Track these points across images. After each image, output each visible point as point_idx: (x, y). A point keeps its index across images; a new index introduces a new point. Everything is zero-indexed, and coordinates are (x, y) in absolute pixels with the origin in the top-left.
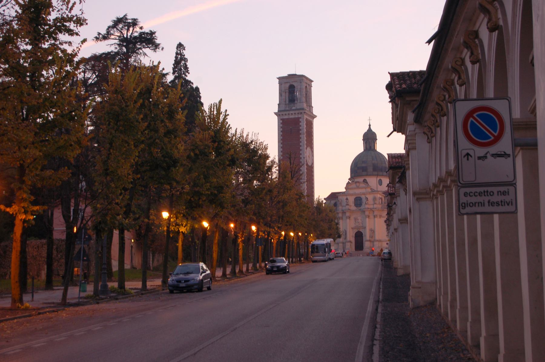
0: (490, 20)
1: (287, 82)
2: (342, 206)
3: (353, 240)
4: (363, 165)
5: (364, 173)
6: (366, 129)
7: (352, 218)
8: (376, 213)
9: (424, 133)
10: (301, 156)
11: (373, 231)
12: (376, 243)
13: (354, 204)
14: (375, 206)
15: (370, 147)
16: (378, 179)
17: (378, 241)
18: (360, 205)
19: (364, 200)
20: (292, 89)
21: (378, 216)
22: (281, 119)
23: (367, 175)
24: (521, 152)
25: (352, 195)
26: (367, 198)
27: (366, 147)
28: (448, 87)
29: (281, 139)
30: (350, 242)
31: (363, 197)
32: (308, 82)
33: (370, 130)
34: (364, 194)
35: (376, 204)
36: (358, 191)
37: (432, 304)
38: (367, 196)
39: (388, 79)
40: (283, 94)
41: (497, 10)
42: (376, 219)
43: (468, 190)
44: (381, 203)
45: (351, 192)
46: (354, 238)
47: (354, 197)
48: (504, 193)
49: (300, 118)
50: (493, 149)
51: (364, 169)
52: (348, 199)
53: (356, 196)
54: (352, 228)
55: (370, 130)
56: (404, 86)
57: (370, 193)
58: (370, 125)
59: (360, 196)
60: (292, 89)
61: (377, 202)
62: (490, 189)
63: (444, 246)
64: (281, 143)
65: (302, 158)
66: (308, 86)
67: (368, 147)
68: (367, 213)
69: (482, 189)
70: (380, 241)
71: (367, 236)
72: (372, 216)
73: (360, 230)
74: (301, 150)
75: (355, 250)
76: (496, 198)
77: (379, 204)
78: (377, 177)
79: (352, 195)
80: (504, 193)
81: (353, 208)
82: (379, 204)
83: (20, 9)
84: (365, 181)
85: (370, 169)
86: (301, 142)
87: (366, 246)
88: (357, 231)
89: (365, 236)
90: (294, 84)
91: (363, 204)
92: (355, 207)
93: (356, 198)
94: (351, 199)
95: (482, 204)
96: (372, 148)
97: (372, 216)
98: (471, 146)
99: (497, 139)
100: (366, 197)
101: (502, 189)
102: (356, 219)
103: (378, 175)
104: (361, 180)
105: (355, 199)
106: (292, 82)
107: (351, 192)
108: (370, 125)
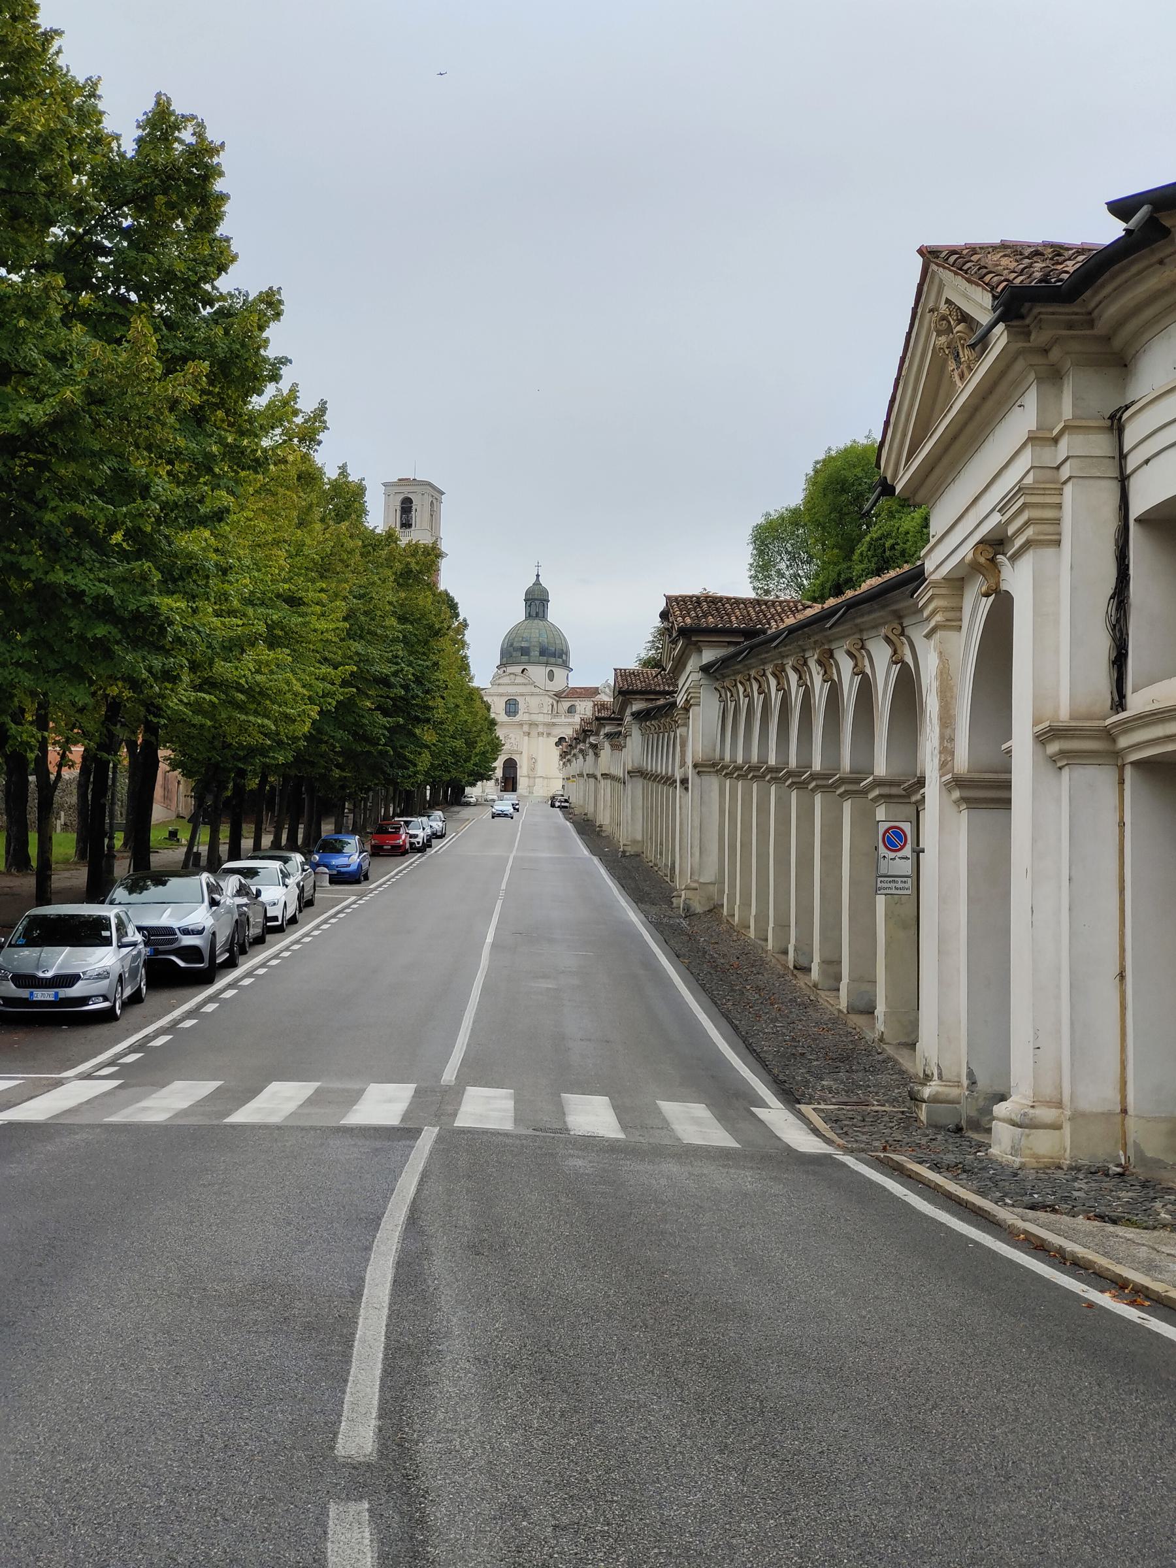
0: (856, 665)
4: (524, 644)
5: (525, 658)
9: (716, 689)
11: (533, 761)
15: (537, 614)
16: (548, 669)
18: (515, 713)
23: (529, 662)
25: (501, 695)
28: (777, 673)
32: (436, 495)
33: (537, 583)
34: (522, 695)
36: (512, 690)
37: (714, 910)
39: (662, 605)
41: (863, 657)
42: (541, 738)
43: (882, 879)
45: (501, 690)
48: (905, 882)
50: (900, 854)
51: (525, 651)
55: (537, 583)
56: (688, 620)
58: (538, 576)
62: (896, 879)
63: (746, 845)
66: (434, 501)
69: (891, 879)
76: (900, 885)
79: (501, 695)
80: (905, 882)
85: (535, 653)
95: (891, 889)
96: (541, 615)
98: (887, 851)
99: (903, 847)
101: (903, 879)
103: (547, 664)
107: (501, 690)
108: (538, 576)
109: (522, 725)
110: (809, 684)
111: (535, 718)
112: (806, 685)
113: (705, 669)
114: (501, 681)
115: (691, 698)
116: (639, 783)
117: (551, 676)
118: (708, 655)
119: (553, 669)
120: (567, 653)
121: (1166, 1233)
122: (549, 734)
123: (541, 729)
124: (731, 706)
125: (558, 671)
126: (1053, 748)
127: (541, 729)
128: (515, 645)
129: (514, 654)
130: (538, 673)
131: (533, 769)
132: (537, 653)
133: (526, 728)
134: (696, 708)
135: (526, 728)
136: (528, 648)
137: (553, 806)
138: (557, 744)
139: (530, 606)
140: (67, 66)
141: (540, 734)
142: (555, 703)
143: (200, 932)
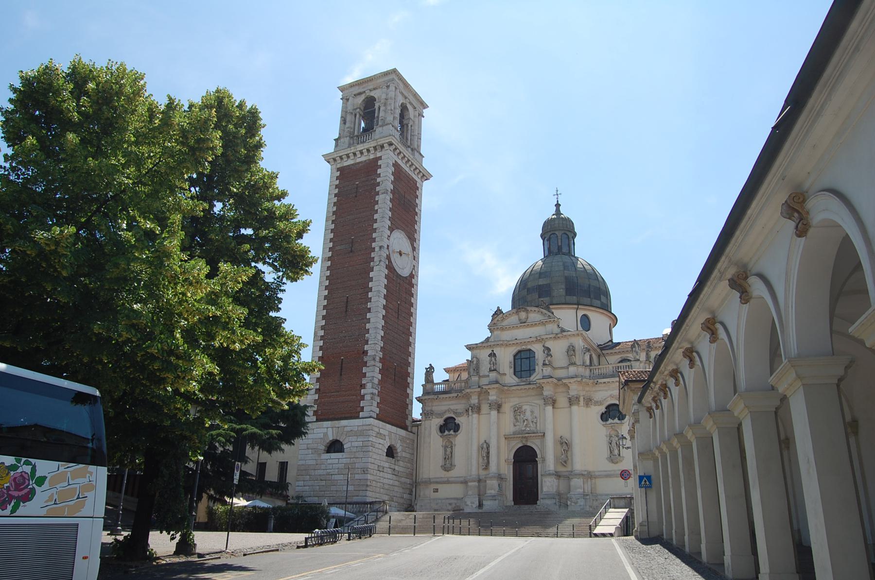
1: (360, 94)
2: (480, 377)
3: (508, 471)
6: (550, 213)
7: (507, 408)
8: (575, 389)
10: (374, 245)
11: (565, 445)
12: (576, 482)
13: (512, 370)
14: (572, 370)
15: (560, 249)
16: (581, 313)
17: (580, 475)
18: (531, 370)
19: (540, 355)
20: (370, 102)
21: (582, 399)
22: (338, 170)
24: (659, 445)
25: (506, 344)
26: (549, 349)
27: (549, 249)
29: (334, 213)
30: (500, 478)
31: (537, 349)
34: (539, 340)
35: (573, 364)
38: (549, 344)
40: (349, 118)
42: (575, 408)
44: (588, 363)
45: (506, 335)
46: (511, 467)
47: (513, 350)
49: (380, 158)
52: (495, 354)
53: (519, 348)
54: (507, 438)
57: (556, 337)
58: (558, 205)
59: (529, 347)
60: (370, 102)
61: (578, 360)
64: (333, 222)
65: (377, 249)
67: (555, 249)
68: (548, 391)
70: (589, 476)
71: (548, 460)
72: (562, 401)
73: (529, 444)
74: (375, 230)
75: (513, 503)
77: (584, 364)
78: (577, 309)
79: (506, 344)
81: (510, 379)
82: (584, 364)
83: (641, 525)
85: (560, 291)
86: (376, 212)
87: (545, 489)
88: (520, 445)
89: (544, 460)
90: (372, 94)
91: (538, 368)
92: (516, 379)
93: (520, 352)
94: (505, 356)
96: (565, 250)
97: (562, 401)
100: (527, 295)
102: (517, 411)
105: (515, 356)
106: (371, 91)
107: (506, 335)
108: (558, 205)
117: (586, 323)
119: (589, 314)
120: (607, 294)
121: (512, 420)
122: (589, 401)
125: (597, 318)
128: (530, 285)
130: (567, 316)
131: (565, 463)
132: (562, 292)
136: (548, 286)
137: (188, 100)
139: (549, 240)
140: (294, 205)
143: (462, 477)
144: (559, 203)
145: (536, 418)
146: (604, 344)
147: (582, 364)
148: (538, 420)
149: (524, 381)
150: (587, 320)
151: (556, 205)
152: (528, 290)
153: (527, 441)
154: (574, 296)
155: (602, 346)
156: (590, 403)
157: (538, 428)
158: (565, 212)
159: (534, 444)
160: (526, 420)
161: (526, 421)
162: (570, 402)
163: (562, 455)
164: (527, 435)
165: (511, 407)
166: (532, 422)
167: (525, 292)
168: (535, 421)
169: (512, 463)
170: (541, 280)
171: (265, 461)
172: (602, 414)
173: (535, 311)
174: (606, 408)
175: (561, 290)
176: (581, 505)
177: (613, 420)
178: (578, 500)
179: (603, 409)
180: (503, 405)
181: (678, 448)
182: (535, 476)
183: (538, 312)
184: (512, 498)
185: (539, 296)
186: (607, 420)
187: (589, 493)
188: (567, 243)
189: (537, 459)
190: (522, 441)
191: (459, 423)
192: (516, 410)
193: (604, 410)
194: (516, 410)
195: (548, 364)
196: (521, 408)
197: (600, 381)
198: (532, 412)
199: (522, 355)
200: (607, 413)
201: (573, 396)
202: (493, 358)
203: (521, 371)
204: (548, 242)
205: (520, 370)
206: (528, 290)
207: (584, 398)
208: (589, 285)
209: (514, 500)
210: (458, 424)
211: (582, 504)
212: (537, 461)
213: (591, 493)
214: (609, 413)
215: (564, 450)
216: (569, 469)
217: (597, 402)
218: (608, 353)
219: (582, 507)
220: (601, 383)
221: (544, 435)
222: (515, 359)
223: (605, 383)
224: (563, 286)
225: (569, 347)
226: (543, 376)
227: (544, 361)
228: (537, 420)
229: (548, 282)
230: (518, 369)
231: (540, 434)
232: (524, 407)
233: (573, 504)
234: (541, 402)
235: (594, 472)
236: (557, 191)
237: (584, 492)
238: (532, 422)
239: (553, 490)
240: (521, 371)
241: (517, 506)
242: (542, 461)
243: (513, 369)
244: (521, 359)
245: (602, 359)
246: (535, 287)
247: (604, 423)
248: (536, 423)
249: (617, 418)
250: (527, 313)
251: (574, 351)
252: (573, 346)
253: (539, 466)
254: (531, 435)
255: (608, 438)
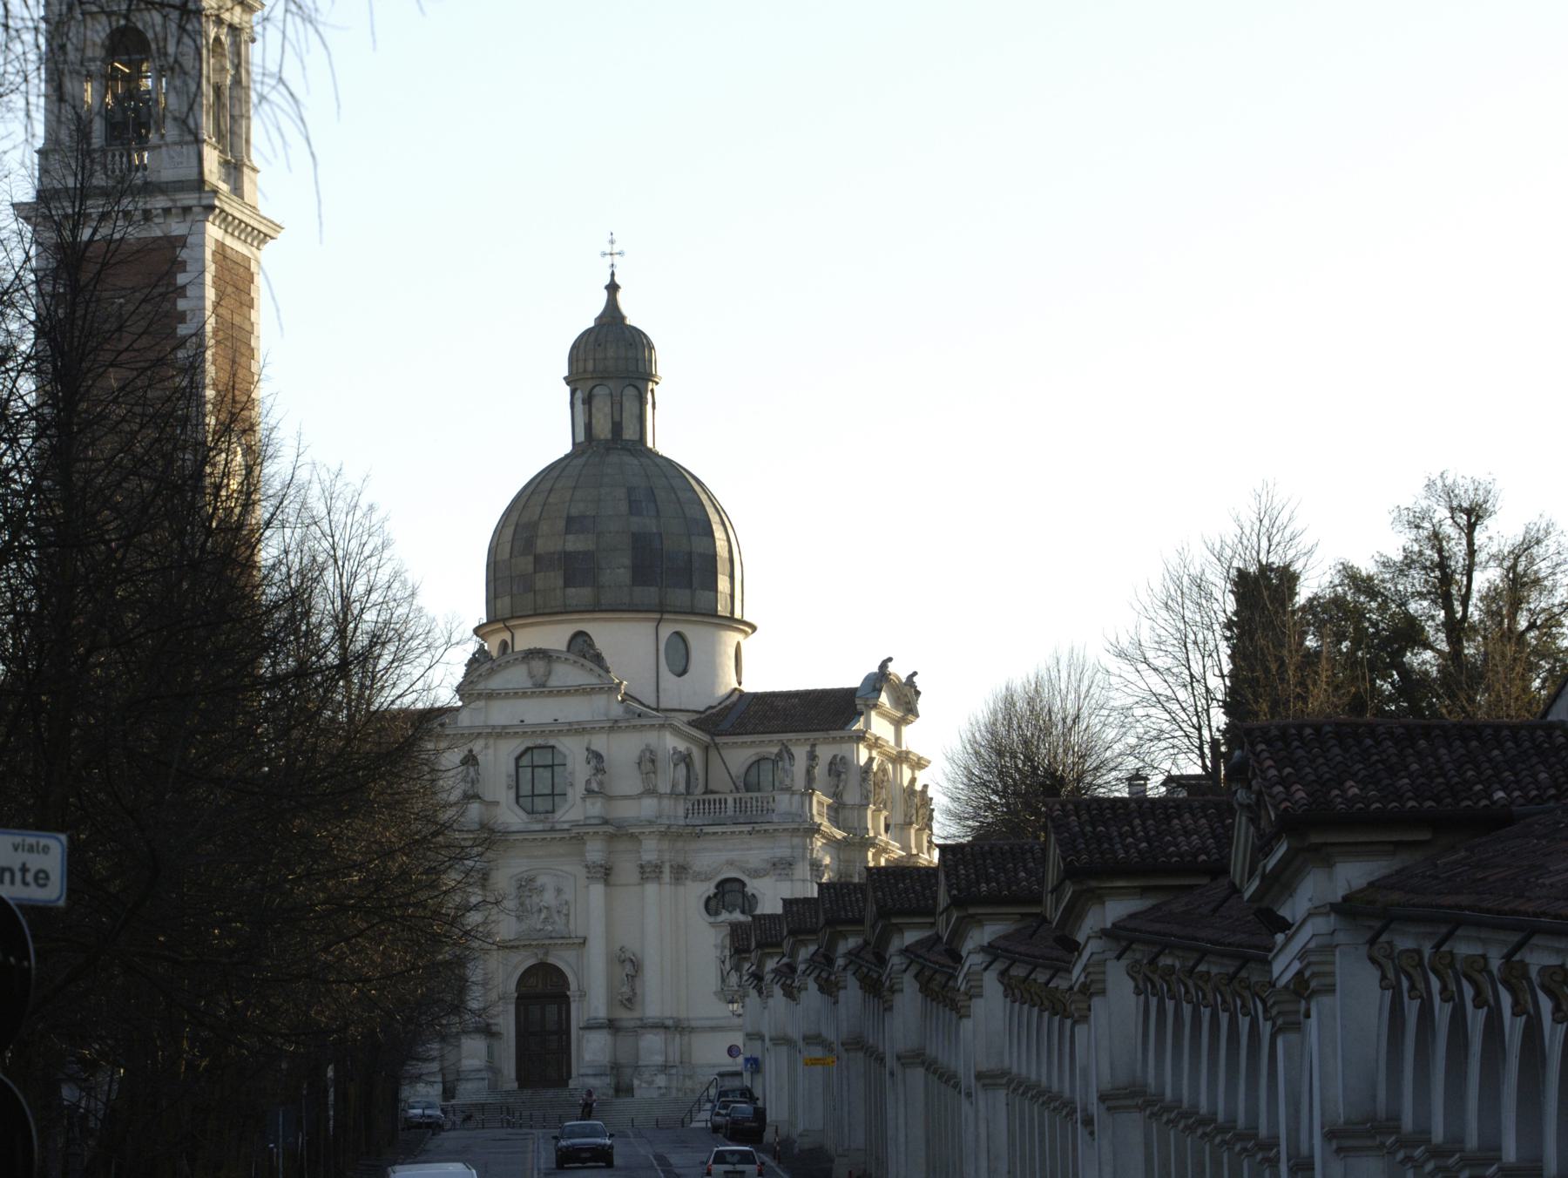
5: (580, 594)
9: (1373, 960)
11: (629, 967)
16: (666, 631)
17: (660, 1026)
19: (579, 770)
21: (667, 870)
23: (597, 608)
26: (598, 756)
27: (589, 427)
31: (573, 749)
33: (612, 317)
35: (651, 792)
36: (538, 712)
42: (651, 889)
44: (682, 788)
45: (500, 713)
51: (577, 569)
53: (530, 744)
55: (612, 317)
57: (614, 727)
58: (613, 288)
59: (552, 742)
70: (676, 1028)
73: (551, 960)
77: (673, 794)
78: (660, 621)
79: (501, 733)
84: (582, 646)
85: (617, 572)
87: (588, 1057)
88: (531, 962)
89: (583, 995)
97: (626, 869)
100: (535, 572)
103: (661, 610)
104: (552, 636)
107: (500, 713)
108: (613, 288)
109: (580, 839)
110: (1532, 1011)
111: (626, 811)
112: (1528, 1014)
113: (1348, 909)
114: (496, 683)
115: (1314, 975)
116: (1133, 1127)
118: (1351, 875)
122: (681, 872)
123: (651, 850)
124: (1412, 1008)
126: (1334, 1144)
127: (651, 850)
129: (540, 582)
131: (629, 1002)
133: (595, 851)
134: (1326, 1000)
135: (595, 851)
138: (712, 906)
141: (650, 873)
142: (697, 755)
144: (618, 280)
145: (567, 903)
146: (720, 704)
147: (668, 791)
148: (572, 910)
149: (541, 821)
150: (681, 645)
151: (607, 287)
152: (538, 559)
153: (546, 954)
154: (651, 585)
155: (714, 711)
156: (684, 876)
157: (572, 927)
158: (634, 314)
159: (562, 959)
160: (547, 908)
161: (545, 911)
162: (642, 873)
163: (623, 985)
164: (547, 942)
165: (511, 878)
166: (558, 912)
167: (526, 564)
168: (565, 911)
169: (514, 1001)
170: (570, 537)
171: (781, 903)
172: (708, 899)
173: (566, 659)
174: (717, 886)
175: (622, 570)
176: (660, 1088)
177: (730, 912)
178: (655, 1078)
179: (709, 888)
180: (494, 874)
181: (223, 238)
182: (564, 1027)
183: (575, 662)
184: (513, 1075)
185: (565, 582)
186: (717, 913)
187: (677, 1064)
188: (636, 411)
189: (568, 993)
190: (536, 954)
191: (755, 892)
192: (521, 886)
193: (712, 891)
194: (521, 886)
195: (596, 789)
196: (532, 880)
197: (706, 830)
198: (559, 891)
199: (535, 758)
200: (719, 896)
201: (649, 862)
202: (471, 769)
203: (533, 795)
204: (587, 406)
205: (530, 793)
206: (538, 559)
207: (671, 866)
208: (690, 554)
209: (518, 1078)
210: (753, 895)
211: (662, 1084)
212: (568, 997)
213: (681, 1062)
214: (723, 896)
215: (627, 975)
216: (636, 1014)
217: (699, 873)
218: (726, 743)
219: (663, 1091)
220: (708, 833)
221: (584, 943)
222: (517, 767)
223: (715, 833)
224: (627, 561)
225: (643, 751)
226: (586, 818)
227: (588, 782)
228: (569, 910)
229: (591, 546)
230: (526, 789)
231: (576, 941)
232: (541, 880)
233: (644, 1085)
234: (581, 872)
235: (688, 1020)
236: (612, 242)
237: (666, 1061)
238: (558, 912)
239: (604, 1059)
240: (533, 795)
241: (528, 1092)
242: (580, 996)
243: (513, 791)
244: (552, 766)
245: (713, 753)
246: (556, 557)
247: (712, 920)
248: (567, 915)
249: (738, 910)
250: (549, 661)
251: (653, 761)
252: (651, 752)
253: (574, 1006)
254: (556, 941)
255: (719, 951)
